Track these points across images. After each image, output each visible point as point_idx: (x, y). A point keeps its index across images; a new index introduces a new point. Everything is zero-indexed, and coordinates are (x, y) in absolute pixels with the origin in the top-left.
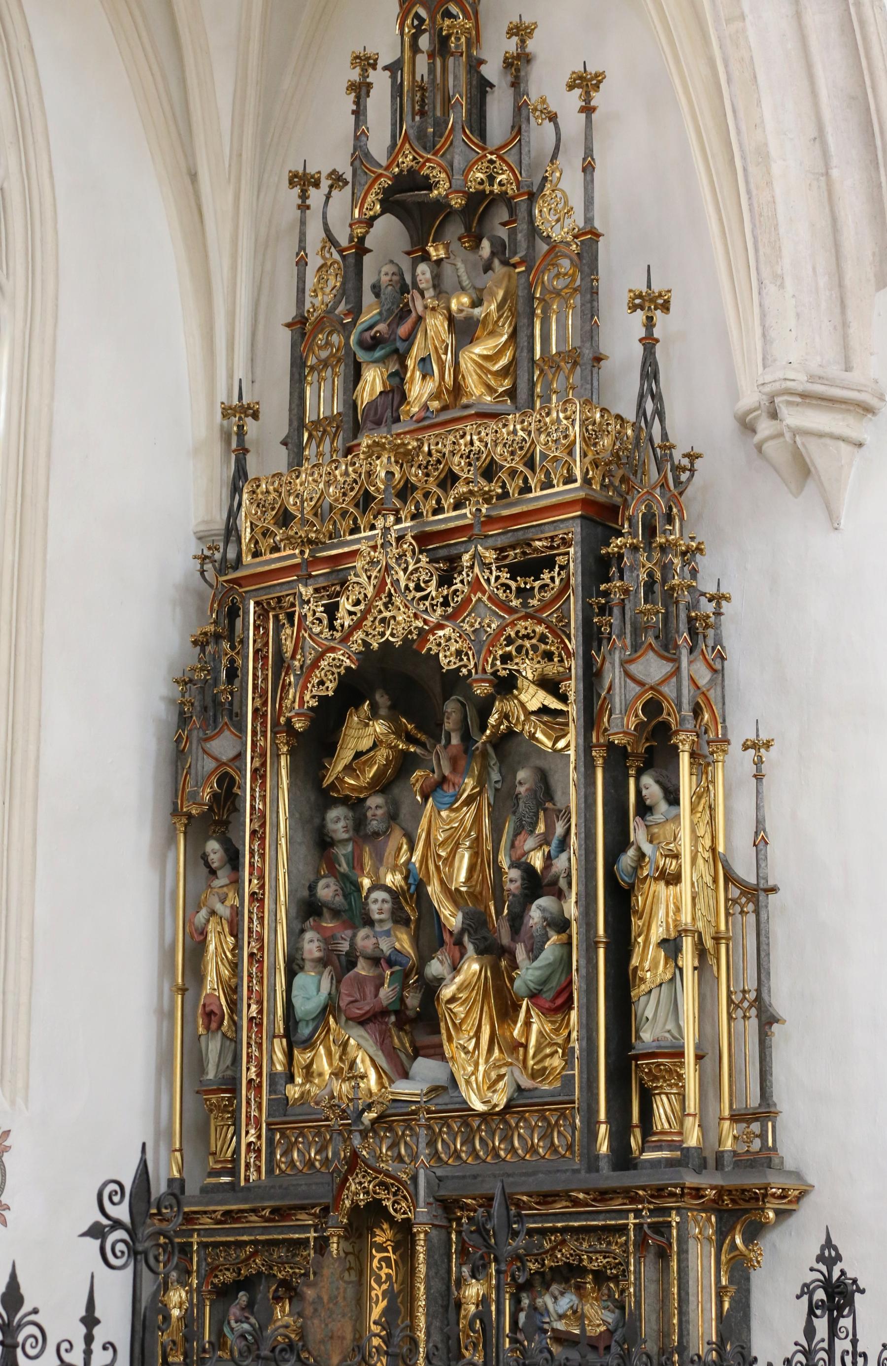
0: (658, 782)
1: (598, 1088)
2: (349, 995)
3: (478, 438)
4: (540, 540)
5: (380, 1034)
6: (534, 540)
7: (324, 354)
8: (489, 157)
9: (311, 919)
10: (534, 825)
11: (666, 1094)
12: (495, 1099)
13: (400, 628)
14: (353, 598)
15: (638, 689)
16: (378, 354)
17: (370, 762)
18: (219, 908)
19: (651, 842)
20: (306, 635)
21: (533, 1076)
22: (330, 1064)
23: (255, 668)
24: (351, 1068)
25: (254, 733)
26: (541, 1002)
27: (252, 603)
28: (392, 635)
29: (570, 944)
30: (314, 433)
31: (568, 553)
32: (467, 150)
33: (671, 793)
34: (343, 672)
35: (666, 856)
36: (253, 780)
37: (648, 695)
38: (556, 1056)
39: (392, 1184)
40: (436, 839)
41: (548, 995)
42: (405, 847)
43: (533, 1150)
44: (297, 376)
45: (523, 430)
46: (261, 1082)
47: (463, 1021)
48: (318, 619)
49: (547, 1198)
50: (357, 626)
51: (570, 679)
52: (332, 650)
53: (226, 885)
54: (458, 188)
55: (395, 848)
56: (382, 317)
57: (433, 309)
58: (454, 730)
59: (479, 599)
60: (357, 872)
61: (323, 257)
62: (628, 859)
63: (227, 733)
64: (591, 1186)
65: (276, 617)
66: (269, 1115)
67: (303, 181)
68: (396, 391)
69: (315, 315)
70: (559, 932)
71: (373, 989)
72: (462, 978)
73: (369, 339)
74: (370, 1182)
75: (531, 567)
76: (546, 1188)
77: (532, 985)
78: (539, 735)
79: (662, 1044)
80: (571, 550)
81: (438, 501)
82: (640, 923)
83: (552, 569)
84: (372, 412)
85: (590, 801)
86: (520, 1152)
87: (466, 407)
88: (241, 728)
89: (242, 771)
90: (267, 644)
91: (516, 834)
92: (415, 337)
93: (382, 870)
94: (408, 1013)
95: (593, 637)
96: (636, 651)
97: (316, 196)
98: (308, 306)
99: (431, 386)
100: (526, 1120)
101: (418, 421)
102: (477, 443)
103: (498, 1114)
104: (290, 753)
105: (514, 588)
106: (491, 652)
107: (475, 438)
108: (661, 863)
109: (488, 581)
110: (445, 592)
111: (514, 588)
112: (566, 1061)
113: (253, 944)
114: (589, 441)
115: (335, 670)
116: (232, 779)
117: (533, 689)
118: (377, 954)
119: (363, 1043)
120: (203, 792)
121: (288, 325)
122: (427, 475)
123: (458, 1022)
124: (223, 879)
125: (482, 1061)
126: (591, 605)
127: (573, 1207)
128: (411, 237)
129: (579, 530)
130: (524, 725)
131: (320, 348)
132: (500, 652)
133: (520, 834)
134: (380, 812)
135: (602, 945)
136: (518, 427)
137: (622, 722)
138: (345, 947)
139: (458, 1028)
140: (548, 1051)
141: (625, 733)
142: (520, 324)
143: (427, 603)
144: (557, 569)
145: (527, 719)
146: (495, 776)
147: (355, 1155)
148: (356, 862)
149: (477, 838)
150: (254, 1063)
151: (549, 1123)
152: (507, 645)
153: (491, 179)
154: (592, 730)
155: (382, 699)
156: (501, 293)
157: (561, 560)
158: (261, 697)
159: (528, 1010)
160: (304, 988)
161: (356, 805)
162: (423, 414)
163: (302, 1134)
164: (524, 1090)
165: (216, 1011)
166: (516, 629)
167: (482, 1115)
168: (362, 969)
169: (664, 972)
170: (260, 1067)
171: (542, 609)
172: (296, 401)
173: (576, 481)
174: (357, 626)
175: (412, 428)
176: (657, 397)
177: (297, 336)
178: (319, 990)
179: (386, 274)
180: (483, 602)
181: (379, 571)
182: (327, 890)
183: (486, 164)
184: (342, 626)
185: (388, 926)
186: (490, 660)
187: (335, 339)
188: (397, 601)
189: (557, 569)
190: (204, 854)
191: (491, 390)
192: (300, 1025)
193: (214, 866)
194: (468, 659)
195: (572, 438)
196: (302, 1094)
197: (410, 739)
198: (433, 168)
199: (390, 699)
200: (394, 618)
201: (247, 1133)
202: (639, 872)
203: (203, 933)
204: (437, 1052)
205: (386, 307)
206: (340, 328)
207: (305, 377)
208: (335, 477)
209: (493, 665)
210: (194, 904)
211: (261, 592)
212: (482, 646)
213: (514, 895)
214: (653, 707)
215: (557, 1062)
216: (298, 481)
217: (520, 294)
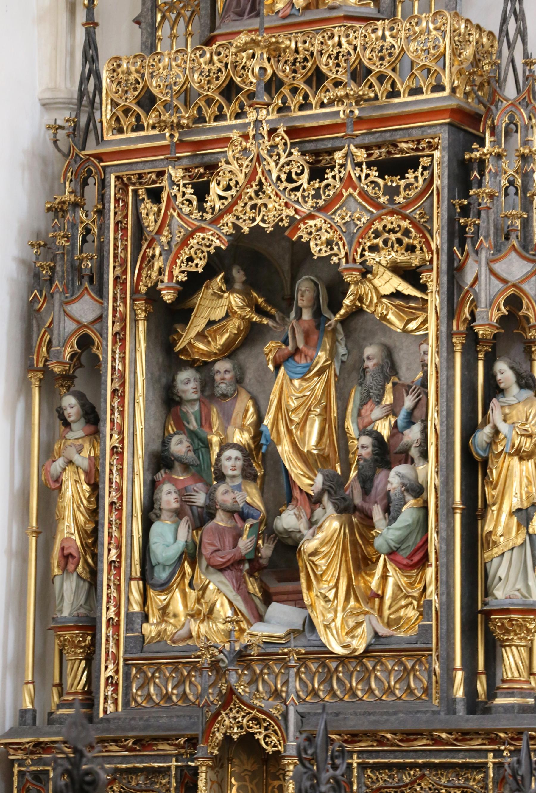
0: (512, 368)
1: (454, 638)
2: (212, 545)
4: (407, 142)
5: (237, 581)
6: (401, 142)
9: (162, 471)
10: (381, 396)
11: (517, 646)
12: (355, 643)
13: (271, 214)
14: (224, 183)
15: (501, 285)
17: (222, 331)
18: (77, 458)
19: (505, 421)
20: (175, 214)
21: (389, 624)
22: (186, 606)
23: (115, 239)
24: (208, 612)
25: (115, 299)
26: (398, 558)
27: (113, 177)
28: (263, 221)
29: (425, 508)
30: (167, 14)
31: (432, 156)
33: (523, 378)
34: (213, 251)
35: (522, 435)
36: (114, 342)
37: (510, 292)
38: (410, 607)
39: (264, 720)
40: (288, 405)
41: (404, 554)
42: (251, 410)
43: (390, 691)
45: (392, 36)
46: (119, 621)
47: (325, 572)
48: (187, 200)
49: (410, 735)
50: (229, 210)
51: (432, 270)
52: (202, 229)
53: (82, 438)
55: (243, 410)
58: (306, 307)
59: (351, 195)
60: (206, 429)
62: (483, 435)
63: (86, 297)
64: (453, 727)
65: (135, 192)
66: (125, 652)
70: (415, 497)
71: (231, 539)
72: (323, 535)
74: (244, 717)
75: (394, 167)
76: (409, 727)
77: (393, 544)
78: (391, 317)
79: (515, 601)
80: (437, 154)
81: (306, 97)
82: (494, 493)
83: (416, 170)
85: (450, 382)
86: (377, 692)
87: (332, 8)
88: (101, 292)
89: (102, 334)
90: (126, 216)
91: (363, 403)
93: (230, 429)
94: (261, 561)
95: (457, 235)
96: (499, 251)
100: (382, 664)
101: (284, 18)
102: (345, 45)
103: (356, 657)
104: (147, 318)
105: (382, 186)
106: (360, 243)
107: (343, 40)
108: (517, 442)
109: (359, 178)
110: (317, 185)
111: (382, 186)
112: (421, 614)
113: (114, 494)
114: (456, 53)
115: (205, 249)
116: (92, 342)
117: (388, 274)
118: (235, 508)
119: (223, 588)
120: (65, 351)
123: (319, 573)
124: (78, 431)
125: (340, 609)
126: (454, 205)
127: (433, 745)
129: (446, 136)
130: (376, 306)
132: (368, 244)
133: (366, 404)
134: (228, 376)
135: (458, 511)
136: (387, 33)
137: (487, 315)
138: (200, 499)
139: (319, 578)
140: (403, 602)
141: (490, 325)
143: (299, 194)
144: (420, 169)
145: (379, 301)
146: (342, 350)
147: (231, 691)
148: (204, 420)
149: (326, 407)
150: (112, 603)
151: (405, 668)
152: (375, 238)
154: (453, 318)
155: (238, 275)
157: (425, 161)
158: (121, 265)
159: (385, 566)
160: (162, 535)
161: (204, 367)
162: (288, 11)
163: (158, 670)
164: (381, 637)
165: (75, 554)
166: (383, 223)
167: (341, 659)
168: (221, 520)
169: (516, 537)
170: (118, 607)
171: (407, 205)
173: (443, 89)
174: (229, 210)
175: (274, 24)
176: (520, 17)
178: (176, 538)
180: (354, 198)
181: (251, 161)
182: (179, 446)
184: (213, 208)
185: (239, 481)
186: (359, 251)
188: (269, 190)
189: (420, 169)
190: (60, 407)
192: (156, 569)
193: (70, 420)
194: (339, 249)
195: (442, 49)
196: (159, 634)
197: (259, 311)
199: (246, 275)
200: (265, 205)
201: (106, 667)
202: (494, 447)
203: (58, 480)
204: (296, 600)
208: (200, 65)
209: (362, 255)
210: (48, 453)
211: (123, 168)
212: (353, 238)
213: (365, 460)
214: (514, 302)
215: (411, 613)
216: (161, 65)
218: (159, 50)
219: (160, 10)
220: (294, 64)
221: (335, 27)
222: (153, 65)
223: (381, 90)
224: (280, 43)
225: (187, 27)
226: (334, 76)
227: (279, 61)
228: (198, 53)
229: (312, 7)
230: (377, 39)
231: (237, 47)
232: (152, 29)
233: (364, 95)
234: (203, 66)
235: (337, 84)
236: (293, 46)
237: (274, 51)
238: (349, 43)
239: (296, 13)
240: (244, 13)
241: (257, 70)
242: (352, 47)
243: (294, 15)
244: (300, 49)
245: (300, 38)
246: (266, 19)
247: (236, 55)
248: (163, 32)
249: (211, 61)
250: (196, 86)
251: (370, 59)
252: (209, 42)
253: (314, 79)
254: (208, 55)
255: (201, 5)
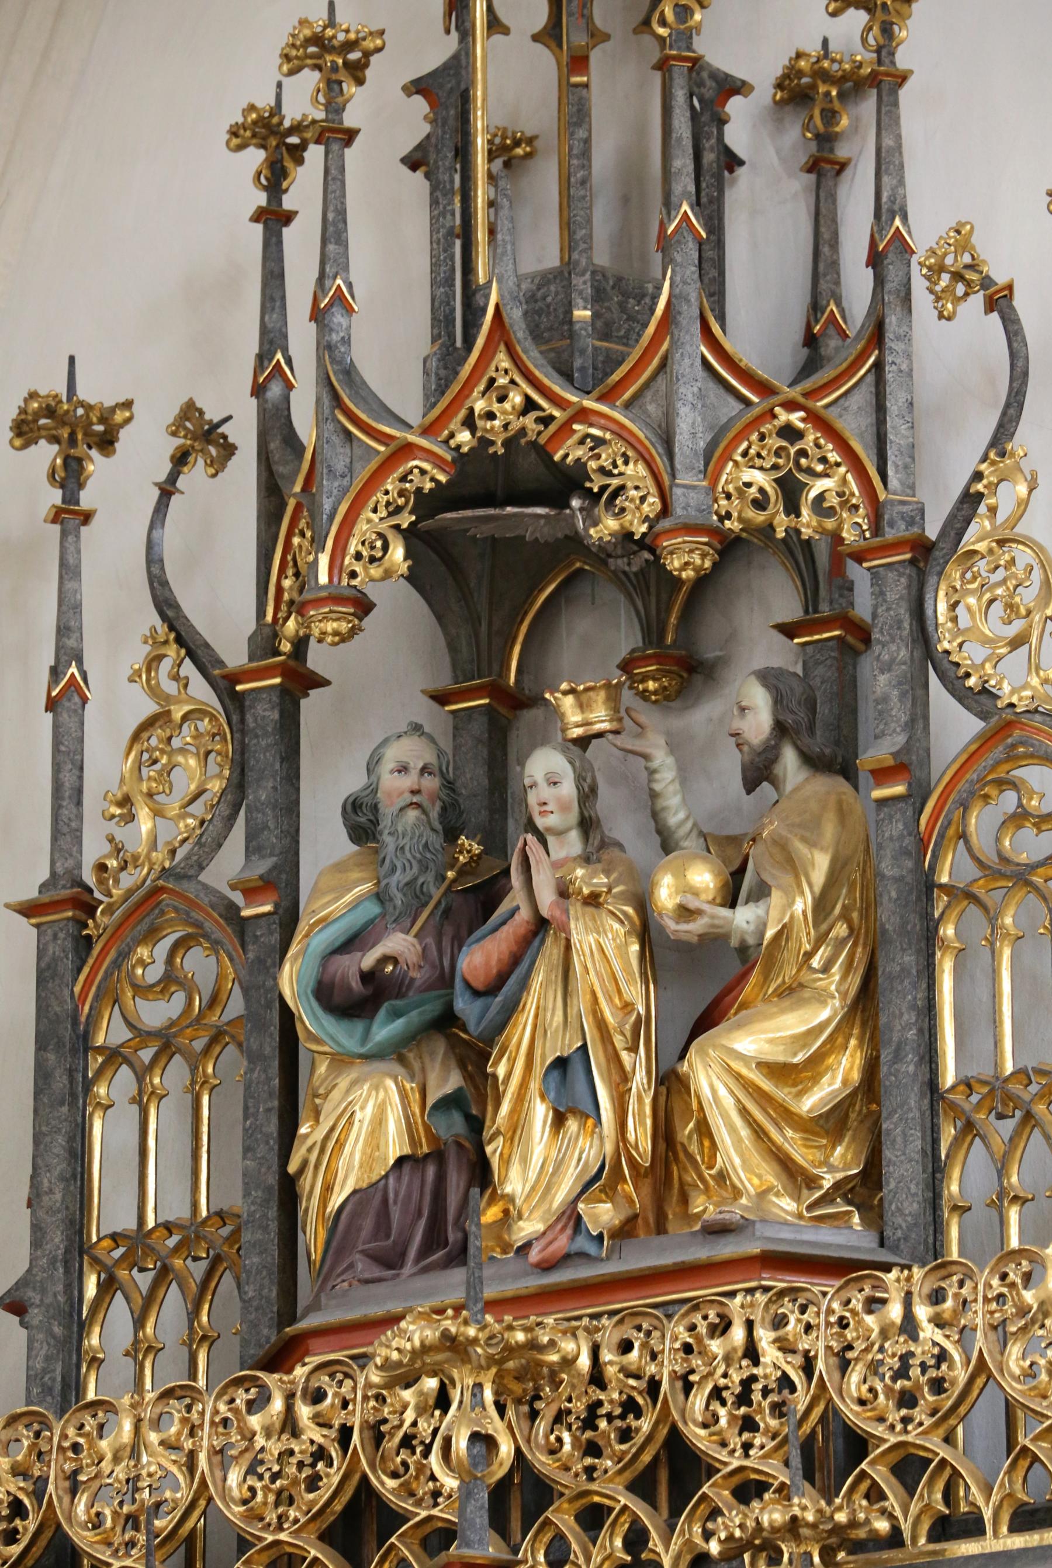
3: (769, 1335)
7: (155, 1013)
8: (784, 416)
16: (385, 1030)
30: (122, 1274)
32: (714, 391)
44: (60, 1082)
45: (939, 1322)
54: (693, 516)
56: (389, 908)
57: (593, 900)
61: (154, 691)
67: (72, 431)
68: (456, 1156)
69: (127, 880)
73: (355, 984)
84: (368, 1224)
87: (718, 1230)
92: (524, 985)
97: (121, 481)
98: (93, 848)
99: (588, 1148)
101: (546, 1266)
102: (770, 1354)
107: (764, 1337)
121: (28, 910)
122: (593, 1449)
128: (452, 647)
131: (141, 990)
136: (922, 1312)
142: (885, 968)
153: (790, 491)
156: (820, 865)
162: (562, 1243)
172: (59, 1165)
177: (62, 947)
179: (403, 769)
183: (775, 442)
187: (198, 963)
191: (796, 1177)
198: (599, 442)
205: (399, 877)
206: (224, 933)
207: (88, 1086)
216: (104, 1444)
217: (888, 868)
218: (91, 1395)
219: (96, 1261)
220: (589, 1422)
221: (732, 1294)
222: (76, 1448)
223: (908, 1512)
224: (541, 1348)
225: (194, 1314)
226: (735, 1463)
227: (534, 1415)
228: (241, 1397)
229: (641, 1233)
230: (884, 1334)
231: (387, 1365)
232: (68, 1327)
233: (853, 1524)
234: (260, 1441)
235: (749, 1490)
236: (584, 1362)
237: (519, 1379)
238: (785, 1347)
239: (591, 1249)
240: (403, 1255)
241: (461, 1444)
242: (798, 1360)
243: (583, 1255)
244: (611, 1371)
245: (610, 1333)
246: (488, 1272)
247: (381, 1399)
248: (110, 1333)
249: (290, 1425)
250: (235, 1512)
251: (862, 1402)
252: (279, 1359)
253: (663, 1476)
254: (277, 1404)
255: (246, 1236)
